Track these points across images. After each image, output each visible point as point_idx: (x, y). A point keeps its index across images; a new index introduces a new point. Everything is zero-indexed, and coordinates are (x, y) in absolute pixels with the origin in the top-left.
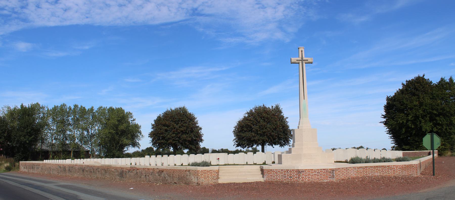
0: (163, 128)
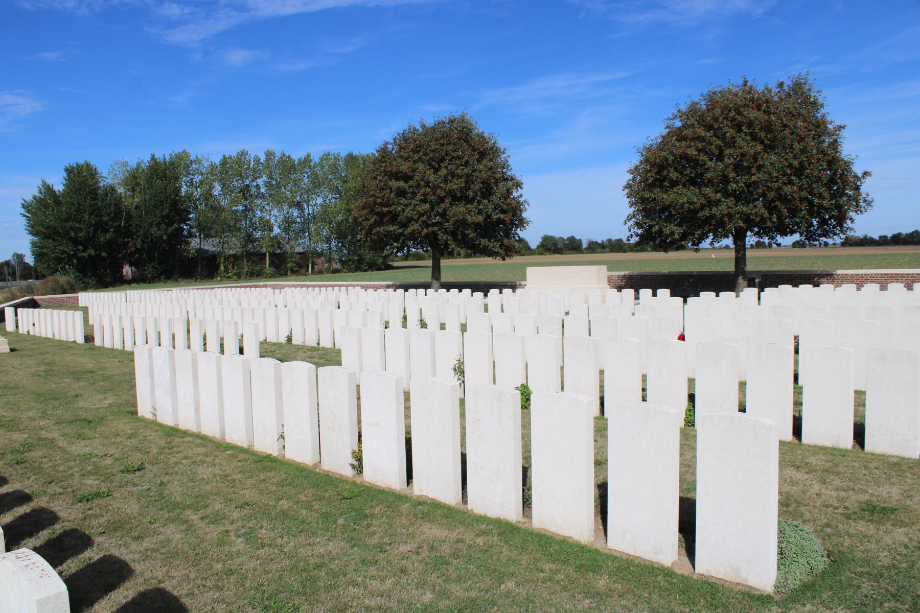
0: (394, 184)
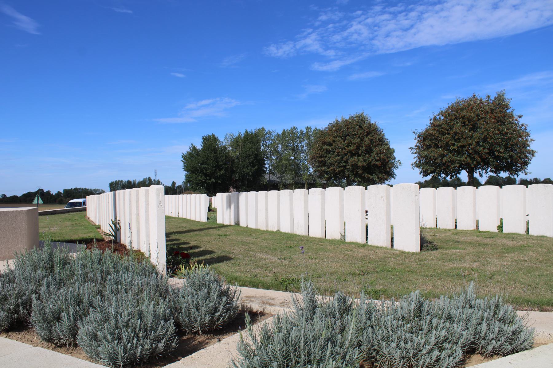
0: (325, 147)
